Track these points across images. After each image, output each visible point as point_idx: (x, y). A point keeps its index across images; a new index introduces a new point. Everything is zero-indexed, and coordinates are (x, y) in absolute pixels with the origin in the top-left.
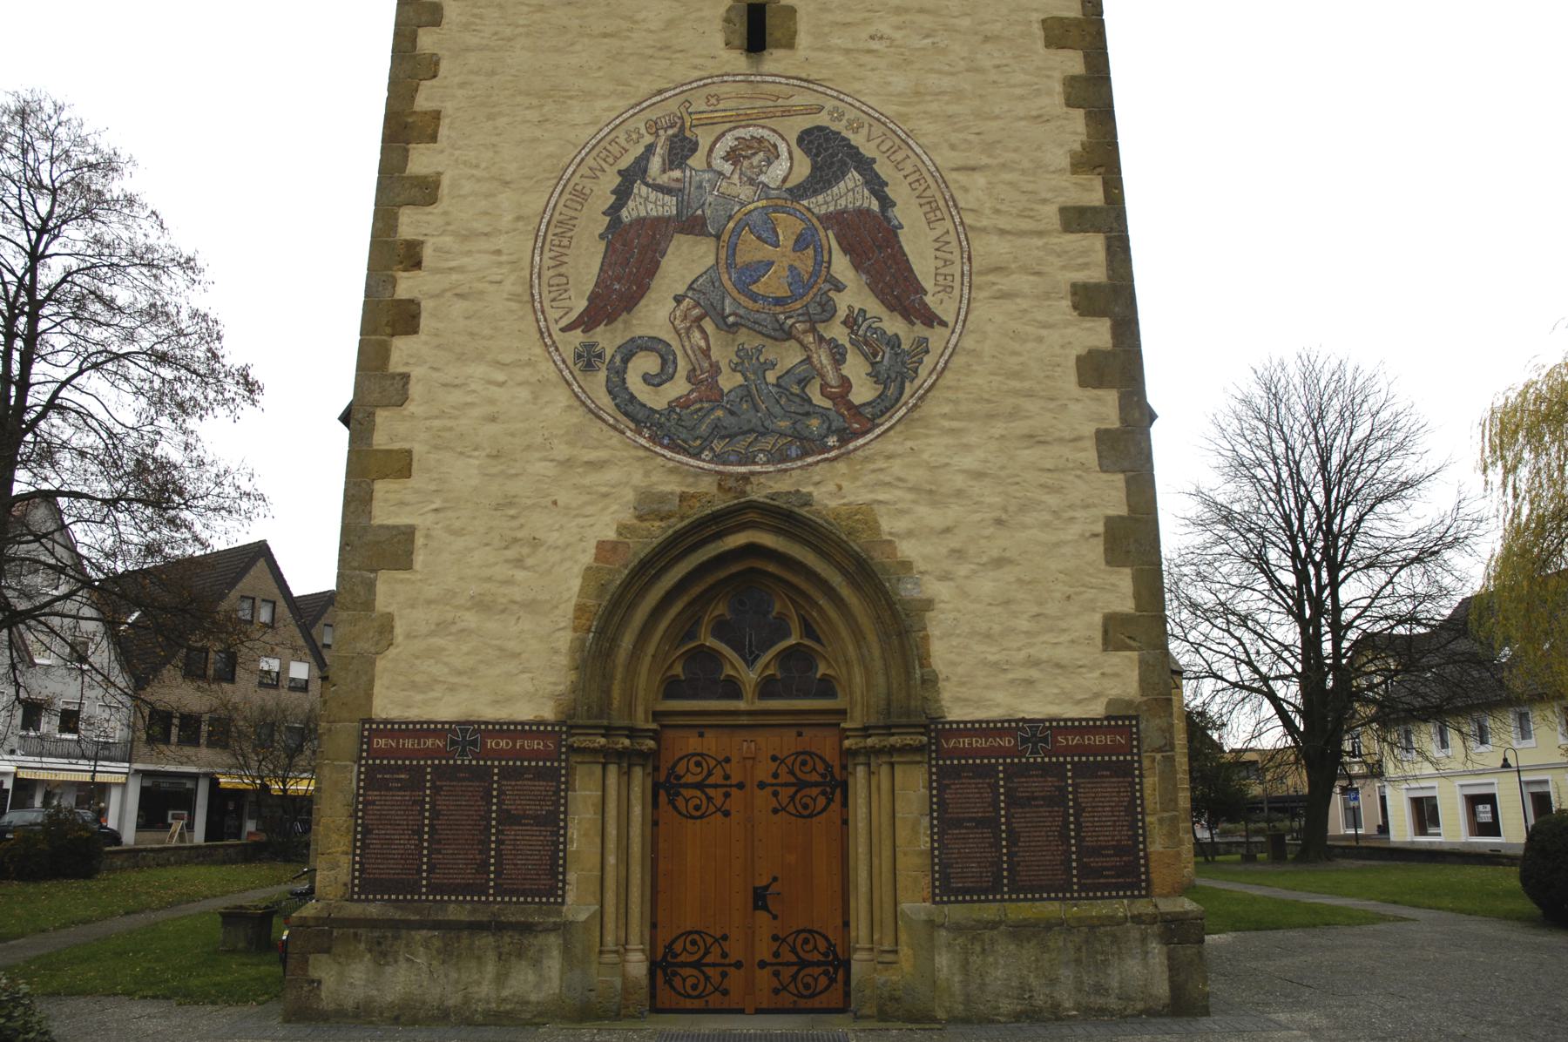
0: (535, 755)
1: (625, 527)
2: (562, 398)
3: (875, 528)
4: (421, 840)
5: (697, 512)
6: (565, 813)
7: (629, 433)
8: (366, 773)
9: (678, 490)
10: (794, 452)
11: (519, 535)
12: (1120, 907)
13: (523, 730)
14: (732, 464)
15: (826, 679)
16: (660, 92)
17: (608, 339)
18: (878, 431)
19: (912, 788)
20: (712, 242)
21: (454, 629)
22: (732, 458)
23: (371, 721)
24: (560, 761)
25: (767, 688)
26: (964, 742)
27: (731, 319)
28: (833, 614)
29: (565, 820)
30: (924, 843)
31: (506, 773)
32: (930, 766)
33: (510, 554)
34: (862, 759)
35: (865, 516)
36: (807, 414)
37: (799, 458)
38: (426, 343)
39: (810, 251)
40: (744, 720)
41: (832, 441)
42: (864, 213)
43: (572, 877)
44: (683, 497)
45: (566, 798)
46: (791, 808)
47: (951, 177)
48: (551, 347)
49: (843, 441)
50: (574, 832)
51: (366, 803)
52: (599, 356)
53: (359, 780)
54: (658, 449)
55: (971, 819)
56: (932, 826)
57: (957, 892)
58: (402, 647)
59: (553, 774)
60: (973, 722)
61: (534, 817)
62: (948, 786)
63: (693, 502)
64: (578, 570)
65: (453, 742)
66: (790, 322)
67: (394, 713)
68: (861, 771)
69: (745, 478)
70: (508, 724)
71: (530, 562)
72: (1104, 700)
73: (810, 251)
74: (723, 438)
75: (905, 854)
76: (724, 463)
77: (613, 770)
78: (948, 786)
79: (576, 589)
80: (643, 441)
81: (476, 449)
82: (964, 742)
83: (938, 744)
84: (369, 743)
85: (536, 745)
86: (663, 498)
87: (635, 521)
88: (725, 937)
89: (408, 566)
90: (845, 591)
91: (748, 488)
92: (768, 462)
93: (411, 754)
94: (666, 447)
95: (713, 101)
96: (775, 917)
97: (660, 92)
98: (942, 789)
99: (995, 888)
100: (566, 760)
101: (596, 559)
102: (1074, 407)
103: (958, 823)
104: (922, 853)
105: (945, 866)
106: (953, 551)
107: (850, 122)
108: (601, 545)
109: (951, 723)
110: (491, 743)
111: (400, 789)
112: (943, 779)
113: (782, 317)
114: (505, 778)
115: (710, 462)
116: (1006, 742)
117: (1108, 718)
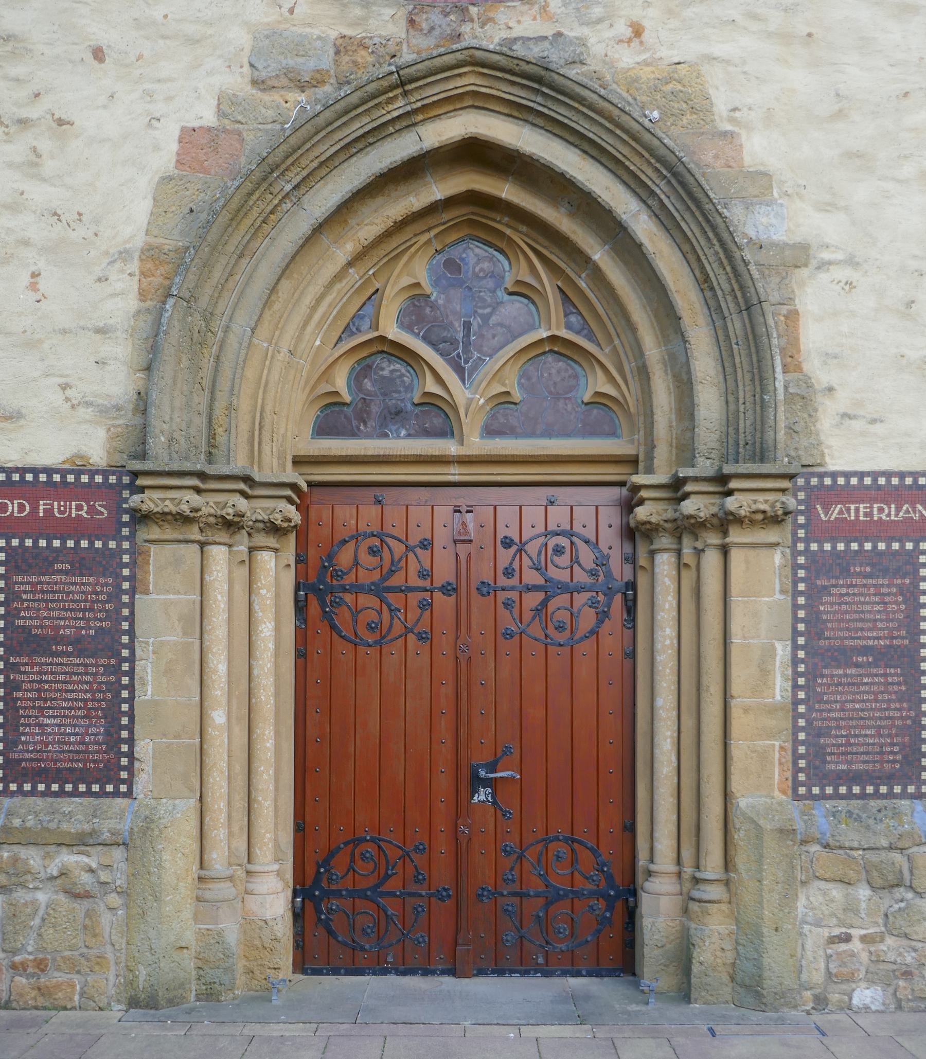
0: (75, 528)
1: (234, 101)
3: (699, 106)
5: (369, 69)
6: (131, 632)
11: (33, 112)
13: (50, 482)
19: (761, 587)
24: (119, 538)
25: (502, 416)
26: (858, 511)
28: (617, 275)
29: (131, 647)
30: (780, 688)
32: (795, 553)
35: (683, 90)
40: (454, 473)
43: (144, 748)
44: (344, 46)
45: (131, 605)
55: (866, 650)
56: (795, 661)
57: (838, 778)
59: (105, 563)
60: (875, 475)
61: (77, 641)
62: (825, 589)
63: (363, 56)
64: (145, 183)
68: (665, 564)
70: (23, 471)
71: (49, 166)
75: (746, 710)
77: (218, 554)
78: (825, 589)
82: (858, 511)
83: (809, 512)
85: (76, 509)
86: (300, 47)
87: (249, 90)
90: (643, 226)
91: (466, 28)
98: (814, 594)
100: (131, 537)
101: (179, 163)
103: (842, 656)
104: (772, 710)
105: (816, 733)
106: (851, 155)
108: (189, 136)
109: (834, 475)
112: (816, 578)
114: (19, 570)
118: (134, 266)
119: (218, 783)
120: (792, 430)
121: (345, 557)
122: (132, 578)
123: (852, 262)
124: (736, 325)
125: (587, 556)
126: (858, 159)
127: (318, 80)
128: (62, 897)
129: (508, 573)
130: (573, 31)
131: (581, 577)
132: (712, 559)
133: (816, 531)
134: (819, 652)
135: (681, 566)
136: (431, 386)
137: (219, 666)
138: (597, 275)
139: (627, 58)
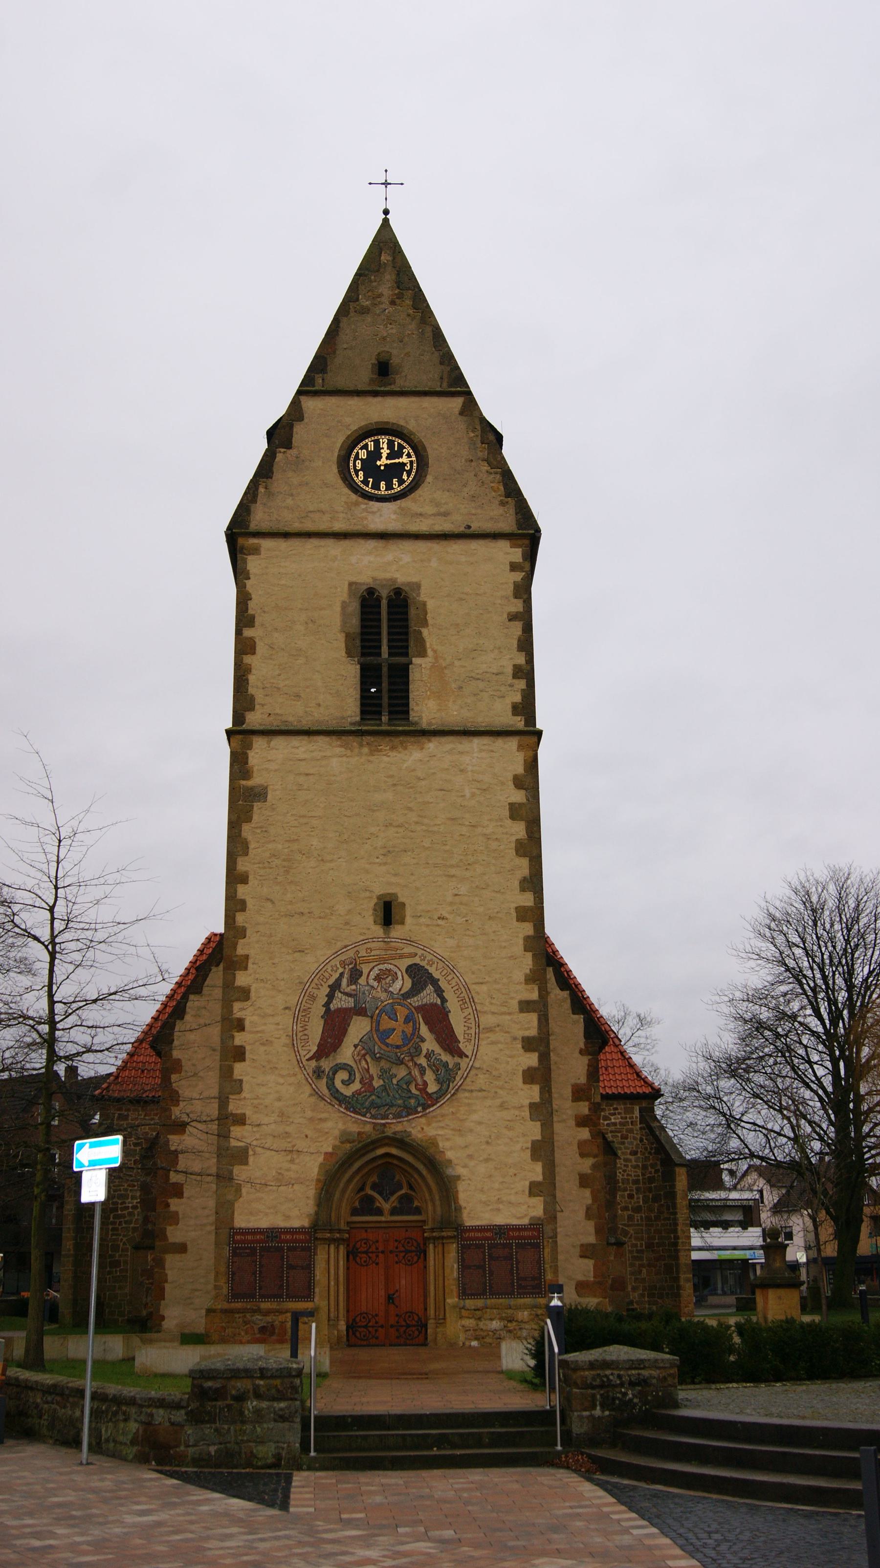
25: (393, 1212)
26: (472, 1234)
30: (455, 1274)
43: (317, 1290)
44: (359, 1133)
59: (308, 1249)
64: (317, 1164)
68: (431, 1246)
71: (297, 1161)
77: (332, 1247)
82: (472, 1234)
86: (350, 1133)
90: (425, 1172)
98: (463, 1253)
112: (463, 1250)
119: (332, 1298)
120: (456, 1217)
121: (358, 1245)
123: (470, 1179)
125: (415, 1244)
126: (470, 1157)
127: (354, 1141)
129: (397, 1248)
130: (409, 1130)
131: (413, 1248)
133: (463, 1239)
134: (464, 1266)
135: (435, 1247)
136: (378, 1204)
137: (332, 1272)
139: (420, 1136)
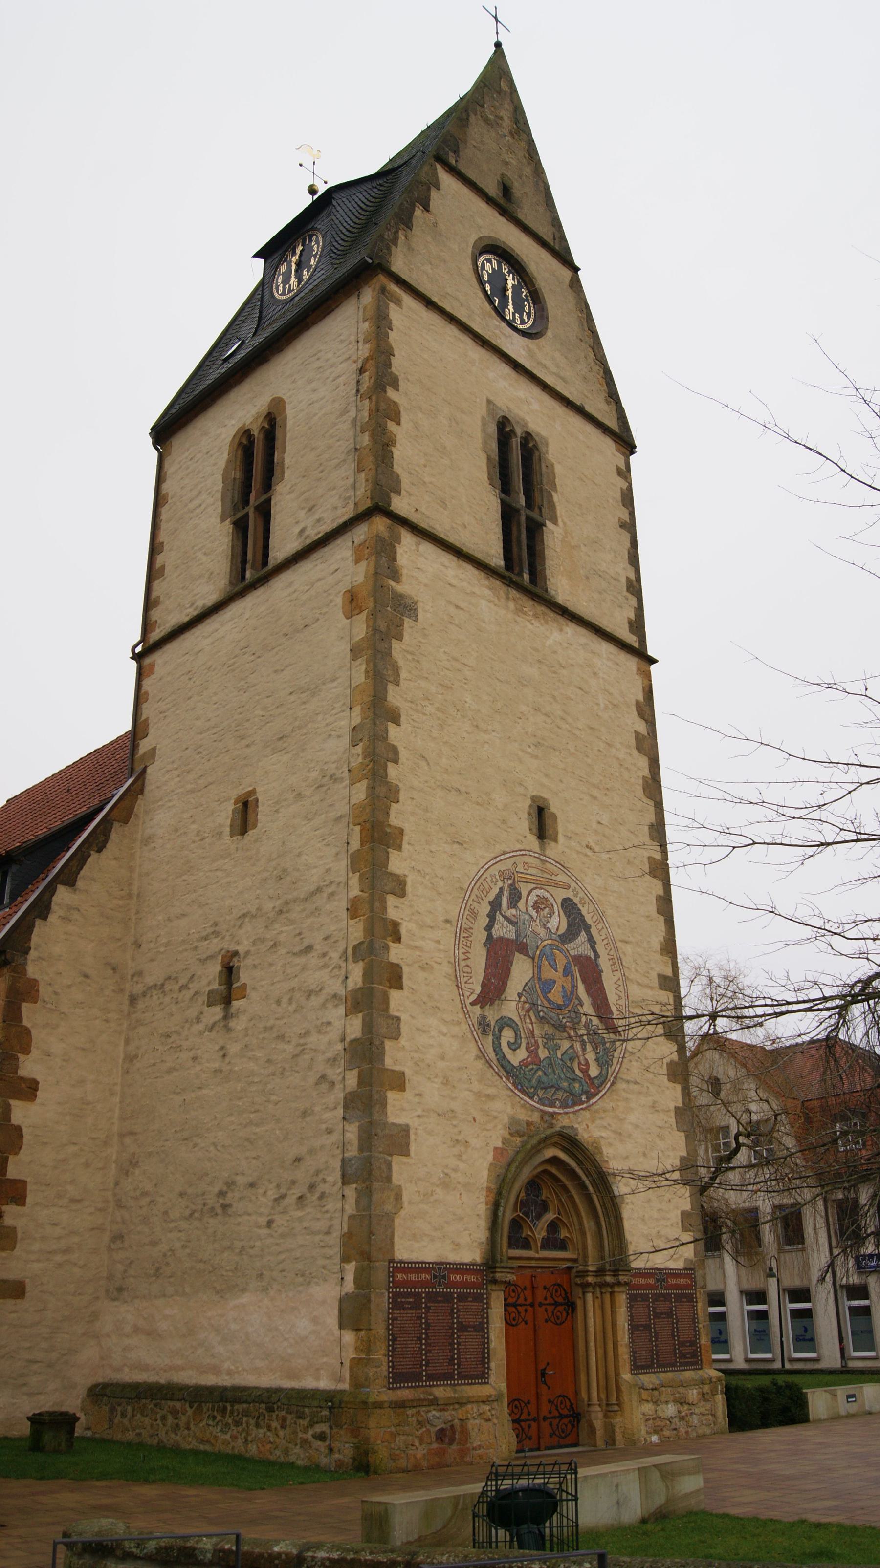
2: (472, 1047)
4: (421, 1344)
7: (504, 1079)
8: (393, 1298)
9: (526, 1118)
10: (570, 1102)
12: (688, 1375)
14: (546, 1106)
15: (563, 1241)
16: (504, 853)
17: (492, 1015)
18: (600, 1095)
20: (529, 960)
21: (432, 1199)
22: (546, 1102)
23: (392, 1261)
24: (483, 1289)
27: (541, 1014)
29: (488, 1328)
31: (462, 1298)
33: (456, 1151)
34: (591, 1289)
36: (574, 1080)
37: (572, 1106)
38: (407, 998)
39: (569, 978)
41: (584, 1098)
42: (588, 958)
43: (493, 1365)
45: (487, 1313)
46: (552, 1319)
47: (620, 944)
48: (466, 1014)
49: (589, 1099)
50: (492, 1336)
51: (394, 1319)
52: (488, 1025)
53: (389, 1303)
54: (516, 1091)
55: (641, 1325)
58: (407, 1209)
61: (474, 1327)
64: (486, 1165)
65: (435, 1277)
66: (564, 1021)
67: (415, 1256)
69: (552, 1115)
71: (464, 1157)
72: (683, 1259)
73: (569, 978)
74: (542, 1089)
76: (544, 1105)
79: (486, 1177)
80: (510, 1085)
81: (436, 1077)
84: (393, 1277)
88: (529, 1403)
89: (407, 1154)
92: (560, 1107)
93: (414, 1285)
94: (519, 1091)
95: (526, 867)
96: (549, 1388)
97: (504, 853)
99: (650, 1366)
102: (667, 1092)
107: (581, 899)
110: (452, 1277)
111: (410, 1309)
112: (632, 1299)
113: (561, 1017)
115: (538, 1103)
116: (651, 1281)
117: (685, 1269)
118: (485, 1193)
122: (487, 1303)
124: (613, 1221)
128: (482, 1421)
132: (607, 1297)
138: (571, 1197)
